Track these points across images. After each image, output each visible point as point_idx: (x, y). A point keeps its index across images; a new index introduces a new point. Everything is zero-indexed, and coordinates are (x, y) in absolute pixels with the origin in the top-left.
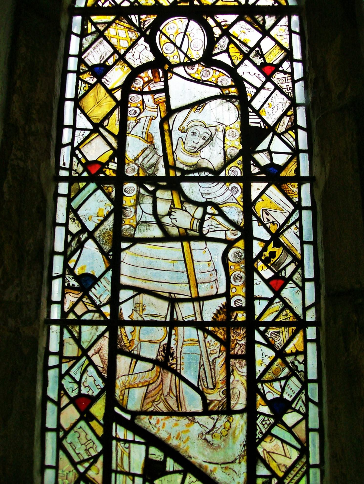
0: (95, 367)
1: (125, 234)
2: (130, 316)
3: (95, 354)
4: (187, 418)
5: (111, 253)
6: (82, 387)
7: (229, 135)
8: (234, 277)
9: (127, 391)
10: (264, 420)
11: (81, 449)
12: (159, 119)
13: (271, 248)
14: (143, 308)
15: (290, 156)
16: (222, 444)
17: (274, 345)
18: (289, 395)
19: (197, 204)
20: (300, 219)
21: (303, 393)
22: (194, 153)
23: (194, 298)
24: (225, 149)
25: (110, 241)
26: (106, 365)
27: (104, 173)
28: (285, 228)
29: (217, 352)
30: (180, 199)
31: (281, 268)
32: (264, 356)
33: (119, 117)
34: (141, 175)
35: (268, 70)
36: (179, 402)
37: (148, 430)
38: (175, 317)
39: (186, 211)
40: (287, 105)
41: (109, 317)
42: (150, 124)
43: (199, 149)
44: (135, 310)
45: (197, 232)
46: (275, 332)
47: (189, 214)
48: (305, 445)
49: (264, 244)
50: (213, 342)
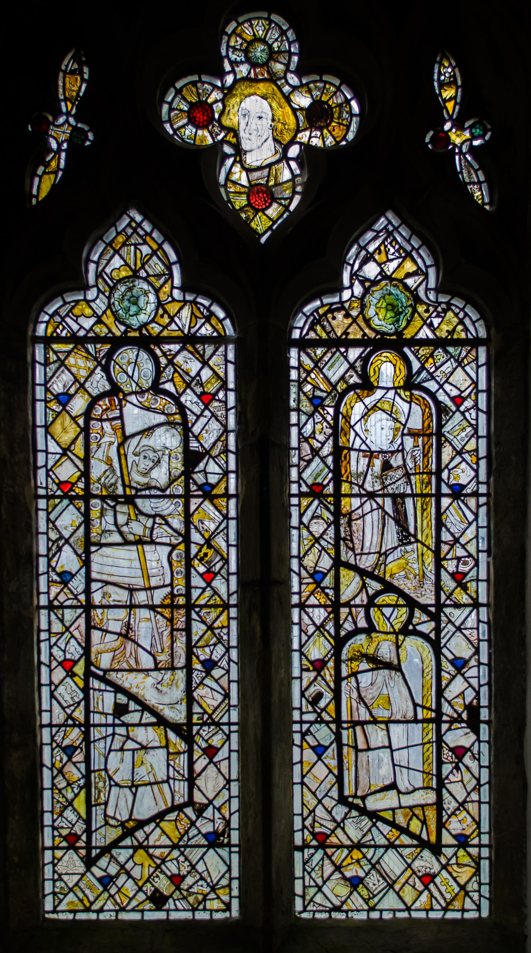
0: (76, 639)
11: (68, 697)
12: (116, 444)
13: (204, 550)
16: (169, 692)
19: (148, 516)
20: (227, 527)
27: (74, 491)
35: (206, 398)
41: (84, 603)
44: (103, 597)
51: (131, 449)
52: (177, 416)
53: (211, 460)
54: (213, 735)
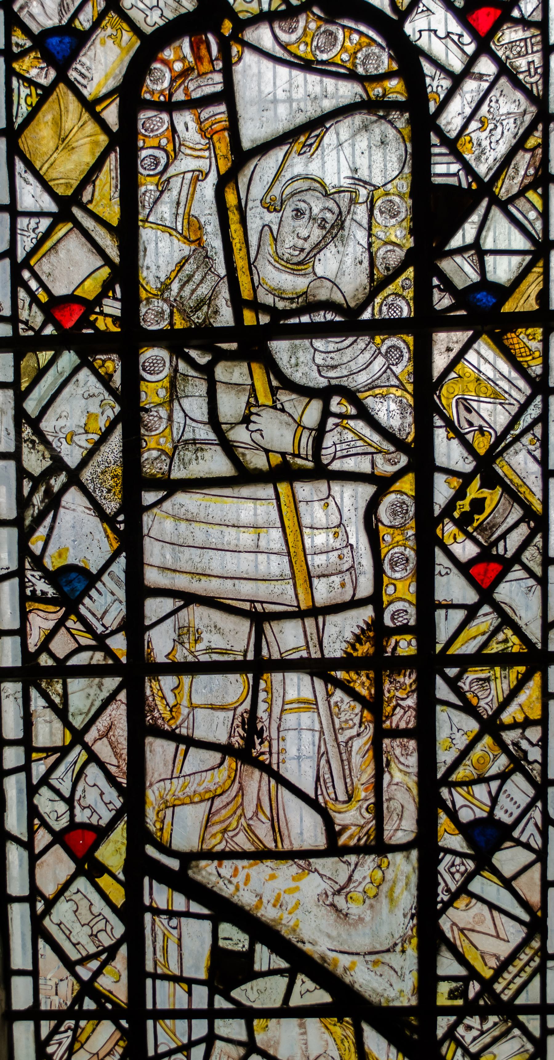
0: (102, 766)
1: (148, 471)
2: (169, 654)
3: (100, 739)
4: (295, 863)
5: (121, 518)
6: (78, 810)
7: (382, 213)
8: (390, 560)
9: (169, 812)
10: (453, 865)
12: (212, 179)
13: (473, 491)
14: (197, 636)
15: (528, 258)
17: (477, 706)
18: (506, 811)
21: (536, 806)
22: (299, 263)
23: (304, 610)
24: (374, 249)
25: (118, 489)
26: (124, 760)
27: (92, 325)
28: (508, 441)
29: (355, 724)
30: (270, 382)
31: (495, 536)
32: (455, 730)
33: (117, 177)
34: (179, 324)
36: (277, 830)
37: (215, 889)
38: (265, 652)
39: (283, 410)
40: (528, 118)
41: (124, 660)
42: (193, 194)
43: (312, 254)
44: (179, 641)
45: (309, 461)
46: (479, 679)
47: (290, 418)
48: (539, 914)
49: (458, 482)
50: (345, 703)
51: (258, 191)
52: (394, 84)
53: (496, 212)
54: (495, 1040)
